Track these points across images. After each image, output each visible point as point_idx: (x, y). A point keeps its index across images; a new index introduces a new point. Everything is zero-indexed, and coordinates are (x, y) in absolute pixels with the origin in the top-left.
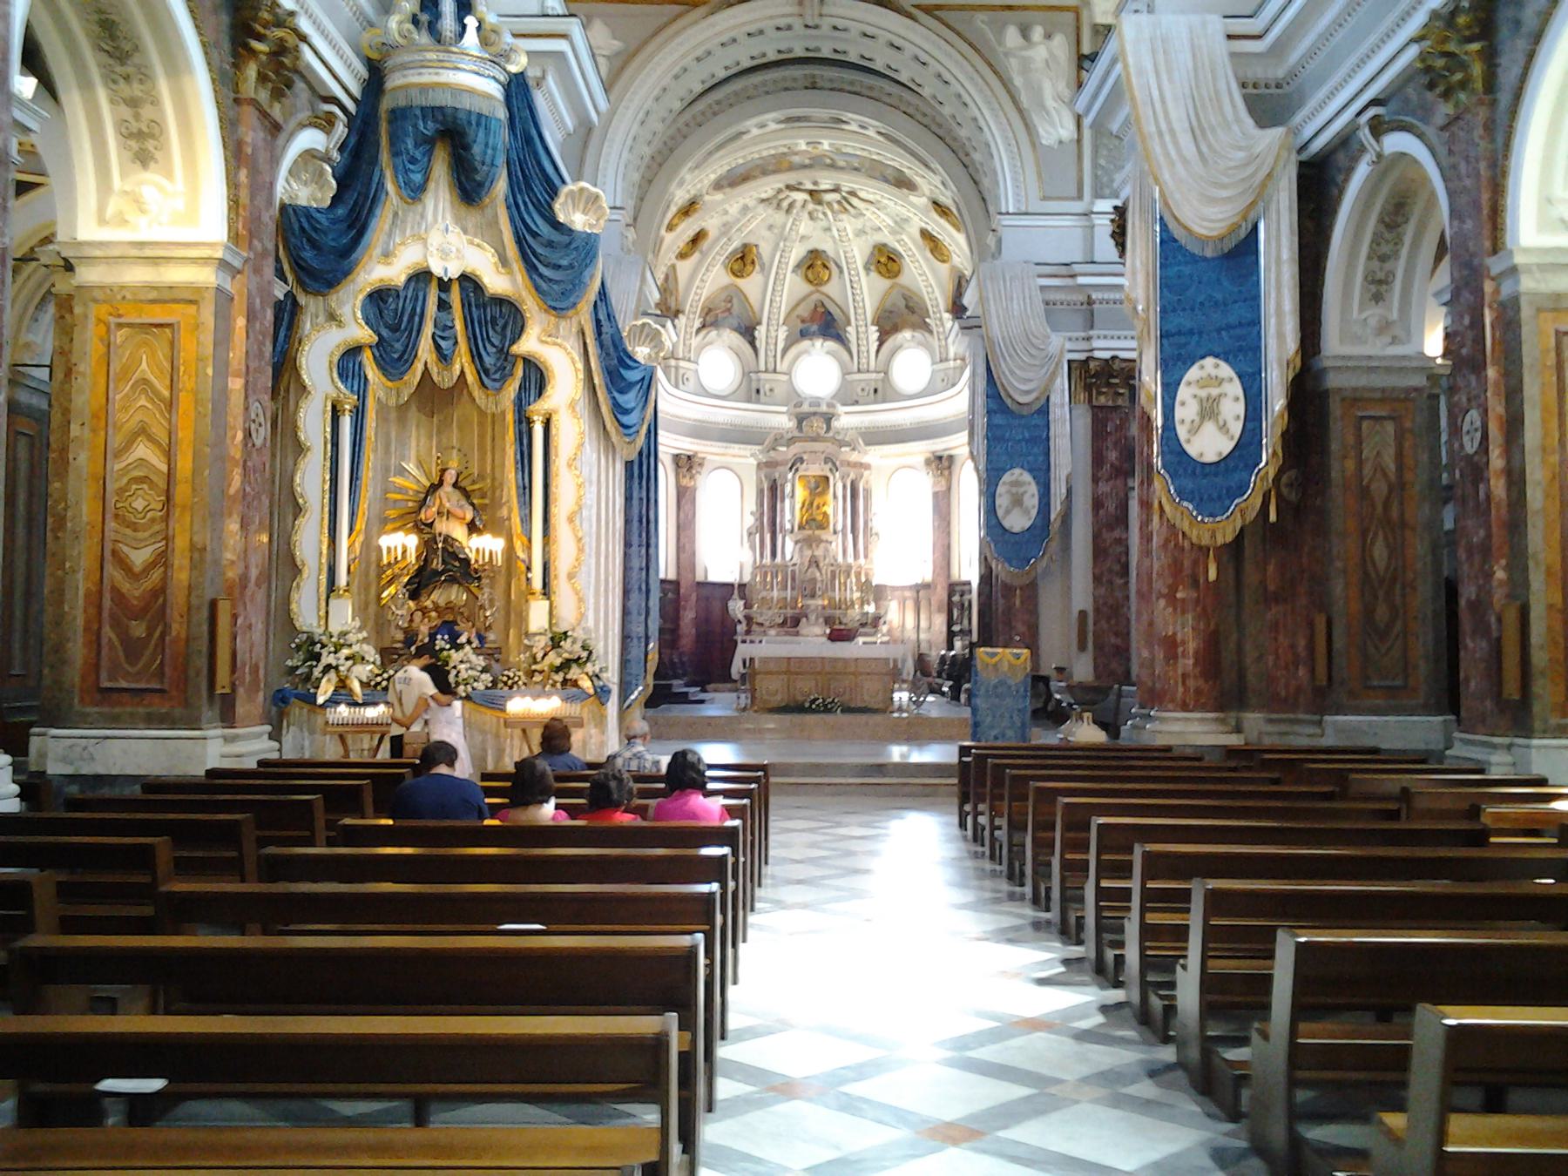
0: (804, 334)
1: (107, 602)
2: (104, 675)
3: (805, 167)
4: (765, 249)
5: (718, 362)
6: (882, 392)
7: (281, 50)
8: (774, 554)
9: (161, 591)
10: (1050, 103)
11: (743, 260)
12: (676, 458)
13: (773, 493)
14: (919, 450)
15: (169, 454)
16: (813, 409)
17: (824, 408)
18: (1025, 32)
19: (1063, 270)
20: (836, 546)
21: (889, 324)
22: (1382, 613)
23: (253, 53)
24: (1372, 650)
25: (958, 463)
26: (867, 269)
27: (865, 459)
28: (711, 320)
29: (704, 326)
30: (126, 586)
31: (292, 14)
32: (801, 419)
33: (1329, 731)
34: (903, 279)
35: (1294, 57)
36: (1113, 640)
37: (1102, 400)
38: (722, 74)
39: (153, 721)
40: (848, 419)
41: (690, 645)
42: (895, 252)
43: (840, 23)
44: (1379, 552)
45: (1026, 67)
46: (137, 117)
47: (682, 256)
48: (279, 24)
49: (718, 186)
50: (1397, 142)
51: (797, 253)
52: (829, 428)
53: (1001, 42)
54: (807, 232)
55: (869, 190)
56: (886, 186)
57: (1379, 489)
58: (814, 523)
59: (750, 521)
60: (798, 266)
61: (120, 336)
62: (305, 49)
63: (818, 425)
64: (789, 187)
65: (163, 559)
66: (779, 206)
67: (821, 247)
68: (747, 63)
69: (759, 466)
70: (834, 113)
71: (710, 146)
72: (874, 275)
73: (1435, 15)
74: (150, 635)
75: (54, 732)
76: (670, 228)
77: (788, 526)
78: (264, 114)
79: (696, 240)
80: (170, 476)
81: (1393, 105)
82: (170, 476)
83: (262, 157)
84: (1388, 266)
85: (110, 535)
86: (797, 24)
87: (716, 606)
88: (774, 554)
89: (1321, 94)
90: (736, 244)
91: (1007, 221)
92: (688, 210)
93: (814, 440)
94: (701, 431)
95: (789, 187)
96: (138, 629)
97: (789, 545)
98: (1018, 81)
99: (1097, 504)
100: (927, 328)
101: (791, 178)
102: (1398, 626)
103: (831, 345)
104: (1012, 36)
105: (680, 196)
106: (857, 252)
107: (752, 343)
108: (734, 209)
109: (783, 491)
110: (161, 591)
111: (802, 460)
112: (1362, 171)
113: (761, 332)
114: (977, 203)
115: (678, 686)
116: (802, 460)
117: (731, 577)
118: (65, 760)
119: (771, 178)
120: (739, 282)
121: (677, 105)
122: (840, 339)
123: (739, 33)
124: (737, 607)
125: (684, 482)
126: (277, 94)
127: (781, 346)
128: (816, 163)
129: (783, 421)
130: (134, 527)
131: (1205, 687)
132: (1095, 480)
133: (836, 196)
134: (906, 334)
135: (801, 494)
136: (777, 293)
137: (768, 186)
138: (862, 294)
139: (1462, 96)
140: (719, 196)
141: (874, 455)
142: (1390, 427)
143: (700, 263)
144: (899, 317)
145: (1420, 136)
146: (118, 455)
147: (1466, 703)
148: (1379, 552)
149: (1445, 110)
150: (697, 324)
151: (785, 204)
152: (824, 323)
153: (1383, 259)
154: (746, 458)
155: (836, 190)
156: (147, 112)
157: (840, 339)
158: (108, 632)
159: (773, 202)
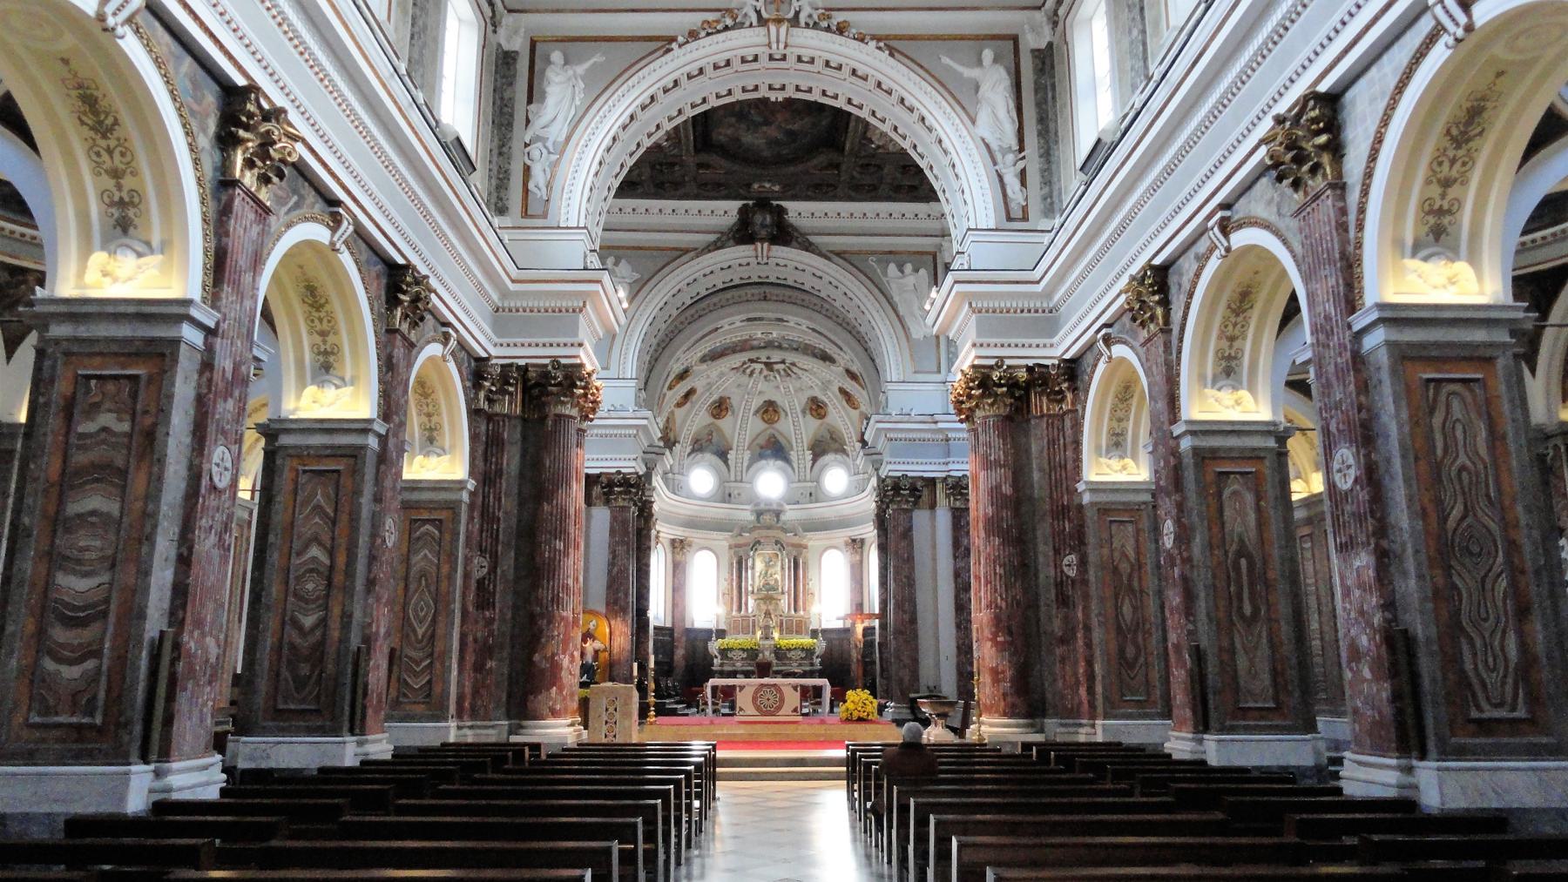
0: (761, 457)
1: (285, 651)
2: (280, 699)
4: (734, 401)
5: (702, 479)
6: (815, 495)
7: (416, 299)
8: (740, 609)
9: (321, 644)
11: (720, 408)
14: (844, 535)
15: (331, 553)
18: (901, 268)
21: (820, 449)
22: (1130, 651)
23: (400, 302)
24: (1125, 676)
26: (804, 412)
27: (804, 542)
28: (698, 447)
30: (298, 641)
31: (426, 277)
32: (759, 514)
33: (1099, 730)
34: (828, 419)
35: (1056, 298)
37: (958, 504)
38: (704, 293)
39: (310, 731)
41: (682, 672)
43: (782, 262)
44: (1127, 609)
46: (325, 342)
47: (679, 405)
48: (417, 282)
49: (703, 360)
50: (1119, 350)
51: (757, 402)
53: (885, 274)
54: (765, 388)
57: (1124, 567)
60: (757, 412)
61: (303, 479)
62: (433, 296)
63: (767, 518)
64: (752, 361)
65: (323, 623)
67: (773, 398)
68: (721, 286)
69: (730, 547)
70: (779, 316)
71: (688, 344)
72: (809, 416)
73: (1133, 278)
74: (312, 672)
75: (244, 739)
76: (670, 388)
78: (405, 338)
79: (689, 394)
80: (332, 568)
81: (1116, 326)
82: (332, 568)
83: (402, 364)
84: (1123, 424)
85: (289, 606)
86: (753, 261)
88: (740, 609)
89: (1074, 319)
90: (715, 397)
91: (890, 386)
93: (769, 528)
94: (693, 523)
95: (752, 361)
96: (304, 669)
97: (751, 602)
98: (896, 299)
100: (844, 451)
101: (753, 355)
102: (1142, 660)
103: (780, 463)
104: (892, 268)
105: (677, 368)
106: (799, 402)
107: (726, 461)
108: (714, 374)
110: (321, 644)
111: (759, 542)
112: (1101, 367)
113: (731, 456)
115: (670, 703)
116: (759, 542)
117: (712, 625)
118: (252, 759)
119: (737, 355)
120: (719, 422)
121: (675, 313)
122: (787, 460)
123: (822, 56)
124: (714, 646)
125: (678, 557)
126: (414, 325)
128: (769, 345)
129: (747, 515)
130: (307, 602)
131: (1018, 701)
132: (955, 557)
136: (743, 428)
137: (737, 360)
138: (798, 429)
139: (1152, 326)
140: (704, 366)
141: (813, 540)
142: (1130, 528)
143: (689, 412)
145: (1132, 348)
146: (299, 554)
147: (1175, 712)
148: (1127, 609)
149: (1144, 334)
150: (689, 450)
152: (775, 449)
153: (1120, 420)
154: (722, 540)
155: (783, 362)
156: (331, 339)
158: (285, 673)
159: (741, 369)
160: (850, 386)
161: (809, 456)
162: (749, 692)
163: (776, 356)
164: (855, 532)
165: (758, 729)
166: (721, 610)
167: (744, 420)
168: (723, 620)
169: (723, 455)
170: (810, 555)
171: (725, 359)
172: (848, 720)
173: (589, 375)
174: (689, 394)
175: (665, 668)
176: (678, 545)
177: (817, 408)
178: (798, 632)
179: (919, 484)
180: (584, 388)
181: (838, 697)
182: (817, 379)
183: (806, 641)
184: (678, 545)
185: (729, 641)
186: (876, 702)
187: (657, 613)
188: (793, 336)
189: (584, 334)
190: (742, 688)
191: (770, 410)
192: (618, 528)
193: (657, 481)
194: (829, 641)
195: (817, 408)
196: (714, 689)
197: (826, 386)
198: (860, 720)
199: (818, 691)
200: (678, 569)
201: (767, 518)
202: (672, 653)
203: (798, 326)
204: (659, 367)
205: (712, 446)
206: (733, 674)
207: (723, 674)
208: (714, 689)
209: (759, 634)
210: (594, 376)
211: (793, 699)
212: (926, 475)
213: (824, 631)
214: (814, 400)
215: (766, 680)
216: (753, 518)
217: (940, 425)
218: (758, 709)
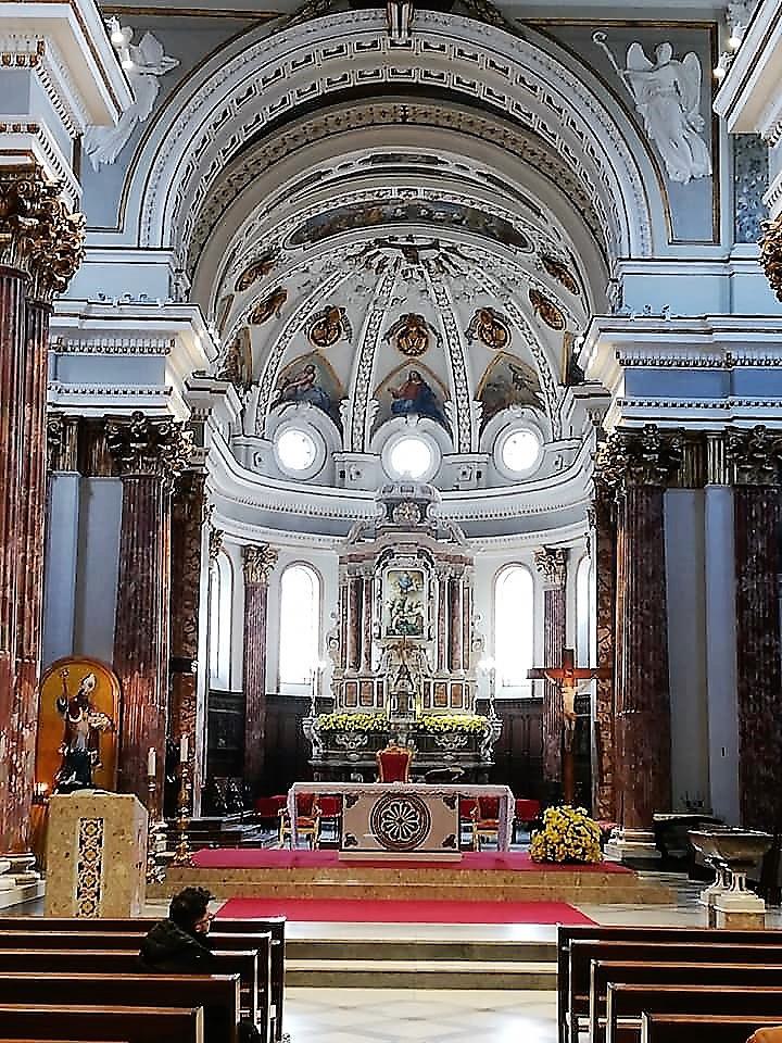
0: (397, 411)
3: (396, 219)
4: (352, 315)
5: (296, 448)
6: (485, 477)
8: (357, 665)
10: (680, 133)
11: (329, 324)
12: (245, 550)
13: (358, 593)
14: (530, 545)
16: (405, 495)
17: (418, 494)
19: (697, 325)
20: (431, 655)
21: (493, 399)
25: (574, 559)
27: (467, 553)
28: (291, 392)
29: (281, 401)
32: (391, 505)
36: (763, 771)
40: (445, 508)
42: (500, 316)
45: (652, 92)
47: (256, 320)
49: (297, 239)
51: (390, 318)
52: (424, 516)
54: (407, 295)
55: (472, 245)
56: (492, 243)
58: (406, 632)
59: (331, 625)
63: (408, 513)
64: (380, 243)
66: (368, 265)
72: (477, 343)
76: (241, 287)
77: (375, 630)
79: (276, 298)
87: (289, 722)
90: (319, 308)
92: (262, 265)
93: (408, 529)
95: (380, 243)
98: (642, 109)
99: (742, 603)
101: (383, 231)
104: (635, 53)
105: (248, 248)
107: (336, 418)
108: (316, 267)
109: (370, 590)
113: (346, 409)
114: (596, 257)
115: (230, 822)
119: (358, 232)
122: (440, 417)
124: (313, 725)
127: (369, 423)
128: (411, 214)
132: (739, 574)
133: (434, 253)
134: (513, 412)
135: (390, 592)
136: (364, 364)
137: (355, 240)
138: (460, 366)
141: (483, 552)
144: (504, 393)
150: (273, 397)
151: (375, 262)
152: (419, 400)
154: (329, 552)
155: (435, 246)
157: (440, 417)
159: (364, 258)
160: (552, 287)
161: (476, 410)
162: (366, 807)
163: (423, 235)
164: (552, 538)
165: (379, 878)
166: (327, 665)
167: (369, 346)
168: (327, 681)
169: (331, 407)
170: (476, 578)
171: (338, 237)
172: (546, 863)
173: (52, 192)
174: (276, 298)
175: (223, 760)
176: (255, 557)
177: (491, 326)
178: (455, 705)
179: (676, 444)
180: (43, 216)
181: (529, 821)
182: (489, 276)
183: (467, 718)
184: (255, 557)
185: (338, 716)
186: (595, 825)
187: (217, 661)
188: (451, 194)
189: (40, 110)
190: (352, 799)
191: (411, 331)
192: (138, 520)
193: (214, 439)
194: (508, 721)
195: (491, 326)
196: (300, 798)
197: (507, 287)
198: (571, 863)
199: (490, 808)
200: (254, 598)
201: (408, 513)
202: (242, 736)
203: (465, 168)
204: (214, 243)
205: (314, 391)
206: (343, 774)
207: (329, 774)
208: (300, 798)
209: (388, 706)
210: (64, 197)
211: (444, 819)
212: (688, 426)
213: (500, 703)
214: (487, 314)
215: (397, 786)
216: (382, 511)
217: (718, 337)
218: (383, 840)
